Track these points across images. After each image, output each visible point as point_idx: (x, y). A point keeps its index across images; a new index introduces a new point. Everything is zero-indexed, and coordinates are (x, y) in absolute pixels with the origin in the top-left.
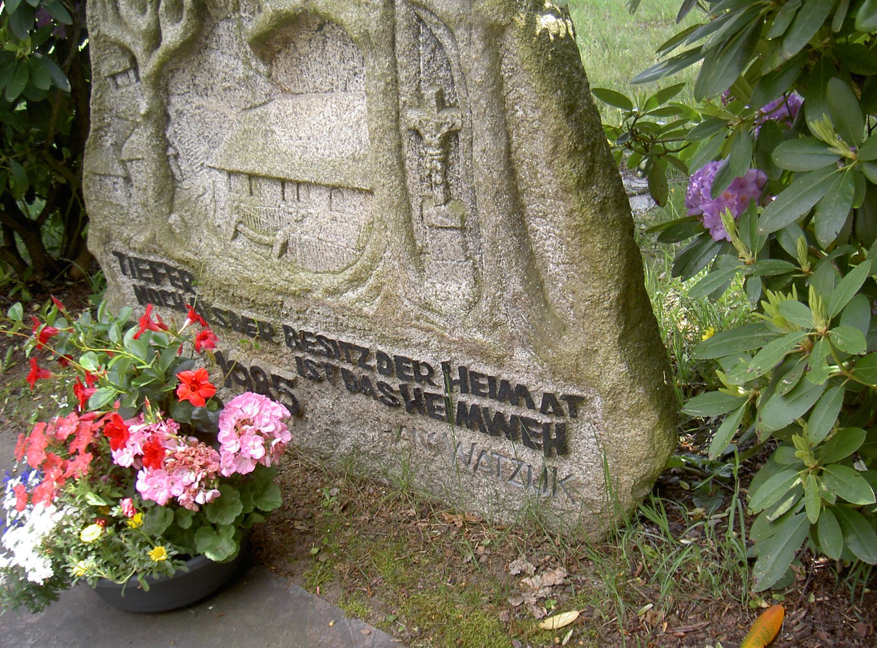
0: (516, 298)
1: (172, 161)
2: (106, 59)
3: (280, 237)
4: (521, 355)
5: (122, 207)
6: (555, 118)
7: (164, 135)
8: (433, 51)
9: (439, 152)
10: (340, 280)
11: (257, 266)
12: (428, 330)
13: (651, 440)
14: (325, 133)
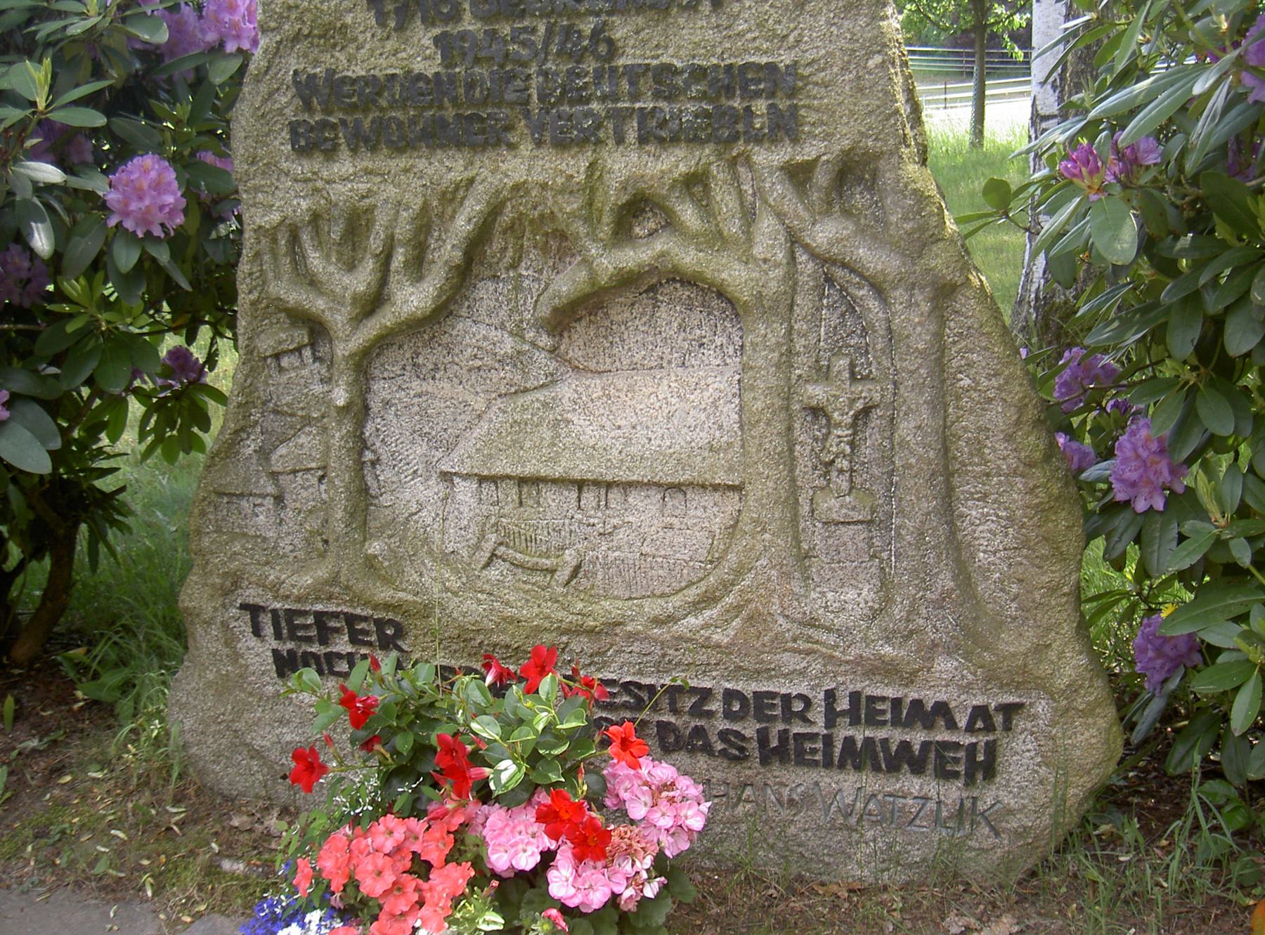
0: (945, 595)
1: (367, 470)
2: (263, 331)
3: (570, 556)
4: (945, 665)
5: (265, 539)
6: (1021, 385)
7: (363, 433)
8: (843, 315)
9: (850, 432)
10: (678, 604)
11: (527, 601)
12: (809, 652)
13: (1107, 741)
14: (660, 418)
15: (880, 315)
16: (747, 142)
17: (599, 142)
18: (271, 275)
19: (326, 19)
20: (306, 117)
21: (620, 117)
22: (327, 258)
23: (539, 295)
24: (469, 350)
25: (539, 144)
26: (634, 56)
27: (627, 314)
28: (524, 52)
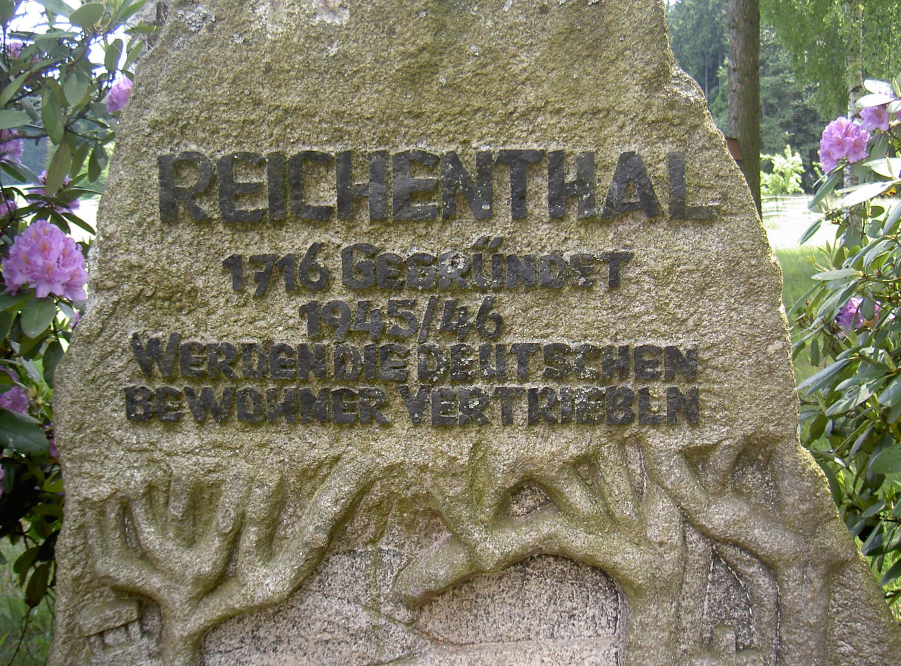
8: (727, 589)
15: (770, 590)
16: (642, 424)
17: (486, 423)
18: (98, 550)
19: (175, 281)
20: (143, 383)
21: (507, 397)
22: (163, 531)
23: (400, 570)
24: (319, 624)
25: (417, 423)
26: (522, 335)
27: (494, 588)
28: (403, 327)
